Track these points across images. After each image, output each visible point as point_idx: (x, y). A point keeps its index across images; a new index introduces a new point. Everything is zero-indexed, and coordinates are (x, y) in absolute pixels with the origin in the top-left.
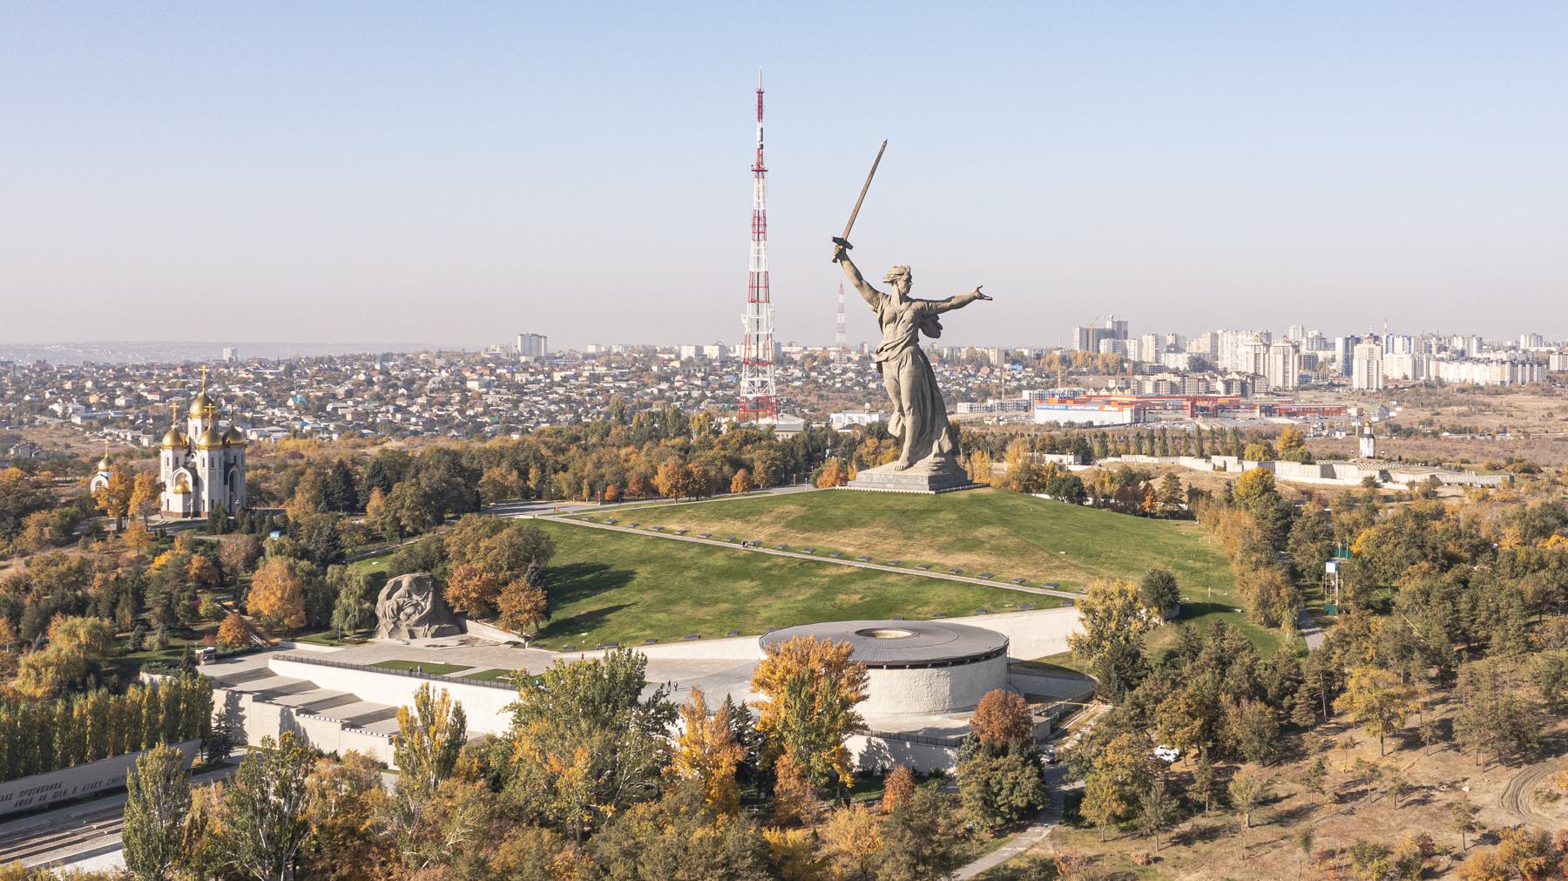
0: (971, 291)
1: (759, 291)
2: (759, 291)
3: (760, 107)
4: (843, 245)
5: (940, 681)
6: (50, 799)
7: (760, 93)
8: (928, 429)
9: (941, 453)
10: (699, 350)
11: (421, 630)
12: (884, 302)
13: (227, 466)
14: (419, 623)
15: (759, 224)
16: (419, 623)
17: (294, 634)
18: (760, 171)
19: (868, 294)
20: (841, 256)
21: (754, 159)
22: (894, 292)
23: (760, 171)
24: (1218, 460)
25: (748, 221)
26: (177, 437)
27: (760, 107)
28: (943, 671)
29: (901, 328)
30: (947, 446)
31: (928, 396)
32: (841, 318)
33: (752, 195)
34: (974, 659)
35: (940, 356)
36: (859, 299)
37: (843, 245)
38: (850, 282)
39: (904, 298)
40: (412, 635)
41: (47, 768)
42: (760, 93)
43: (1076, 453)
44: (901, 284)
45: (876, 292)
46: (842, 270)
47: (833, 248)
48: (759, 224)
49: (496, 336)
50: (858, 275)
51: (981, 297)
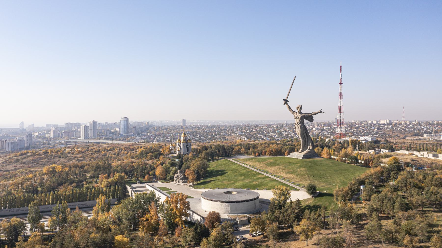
0: (318, 111)
1: (341, 110)
2: (341, 110)
3: (341, 70)
4: (286, 101)
5: (228, 206)
6: (84, 206)
7: (341, 67)
8: (307, 144)
9: (309, 149)
10: (372, 122)
11: (180, 181)
12: (295, 114)
13: (187, 146)
14: (180, 179)
15: (341, 95)
16: (180, 179)
17: (162, 179)
18: (341, 83)
19: (292, 112)
20: (286, 103)
21: (339, 81)
22: (297, 111)
23: (341, 83)
24: (422, 153)
25: (338, 95)
26: (179, 140)
27: (341, 70)
28: (228, 204)
29: (298, 120)
30: (311, 148)
31: (306, 136)
32: (403, 115)
33: (339, 89)
34: (251, 200)
35: (430, 123)
36: (290, 113)
37: (286, 101)
38: (288, 109)
39: (300, 113)
40: (179, 182)
41: (86, 201)
42: (341, 67)
43: (389, 149)
44: (299, 109)
45: (294, 112)
46: (286, 106)
47: (284, 102)
48: (341, 95)
49: (41, 126)
50: (290, 108)
51: (321, 112)
